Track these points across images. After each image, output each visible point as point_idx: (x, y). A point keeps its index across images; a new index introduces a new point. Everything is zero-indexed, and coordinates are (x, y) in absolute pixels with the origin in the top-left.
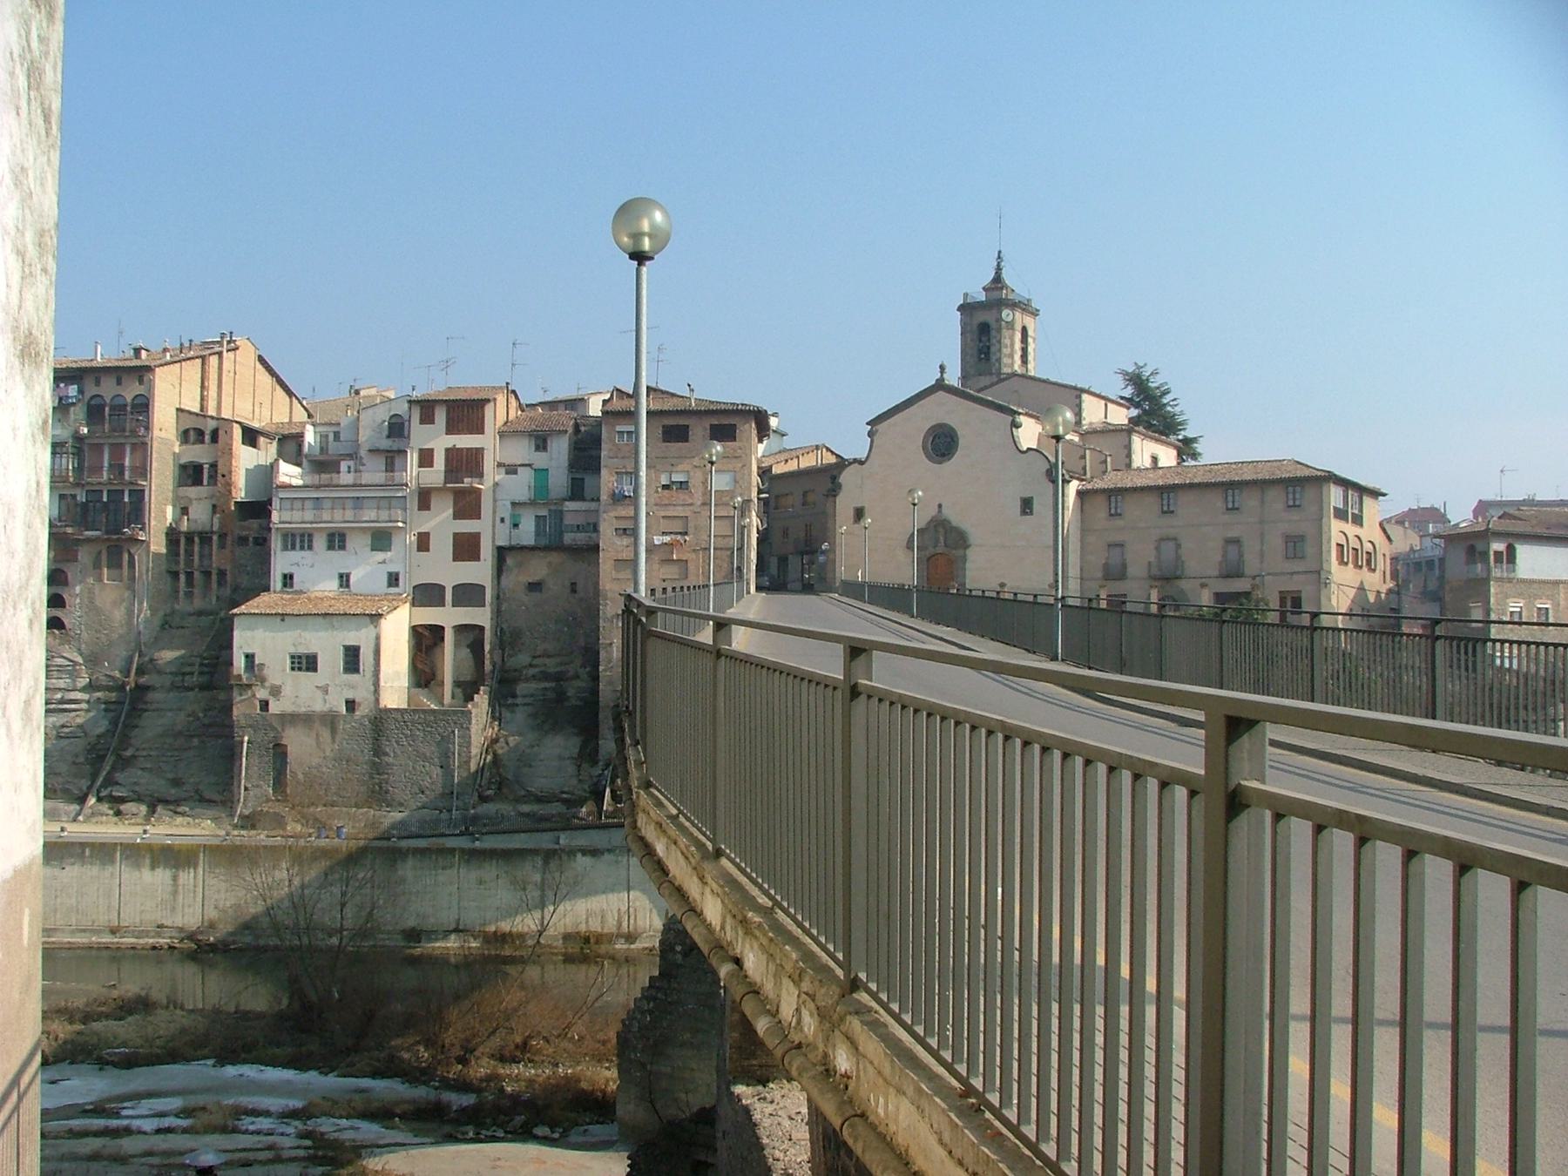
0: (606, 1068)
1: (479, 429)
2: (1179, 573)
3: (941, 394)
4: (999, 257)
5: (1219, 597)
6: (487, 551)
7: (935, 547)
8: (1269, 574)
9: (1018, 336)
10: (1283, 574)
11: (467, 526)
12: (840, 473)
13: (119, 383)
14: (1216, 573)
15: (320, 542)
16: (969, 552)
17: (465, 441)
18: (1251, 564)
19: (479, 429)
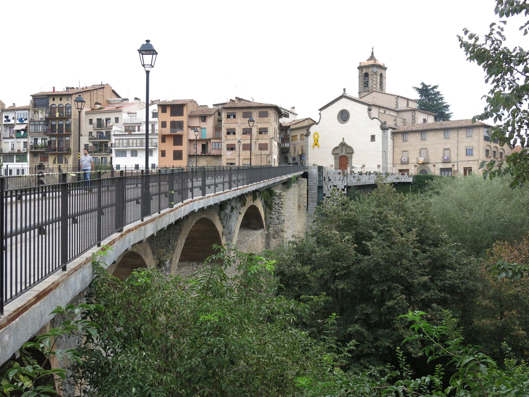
0: (211, 355)
1: (182, 114)
2: (427, 161)
3: (344, 100)
4: (373, 49)
5: (442, 170)
6: (185, 155)
7: (342, 153)
8: (460, 161)
9: (379, 77)
10: (465, 161)
11: (178, 148)
12: (310, 128)
13: (61, 100)
14: (441, 161)
15: (129, 154)
16: (353, 155)
17: (177, 119)
18: (454, 158)
19: (182, 114)
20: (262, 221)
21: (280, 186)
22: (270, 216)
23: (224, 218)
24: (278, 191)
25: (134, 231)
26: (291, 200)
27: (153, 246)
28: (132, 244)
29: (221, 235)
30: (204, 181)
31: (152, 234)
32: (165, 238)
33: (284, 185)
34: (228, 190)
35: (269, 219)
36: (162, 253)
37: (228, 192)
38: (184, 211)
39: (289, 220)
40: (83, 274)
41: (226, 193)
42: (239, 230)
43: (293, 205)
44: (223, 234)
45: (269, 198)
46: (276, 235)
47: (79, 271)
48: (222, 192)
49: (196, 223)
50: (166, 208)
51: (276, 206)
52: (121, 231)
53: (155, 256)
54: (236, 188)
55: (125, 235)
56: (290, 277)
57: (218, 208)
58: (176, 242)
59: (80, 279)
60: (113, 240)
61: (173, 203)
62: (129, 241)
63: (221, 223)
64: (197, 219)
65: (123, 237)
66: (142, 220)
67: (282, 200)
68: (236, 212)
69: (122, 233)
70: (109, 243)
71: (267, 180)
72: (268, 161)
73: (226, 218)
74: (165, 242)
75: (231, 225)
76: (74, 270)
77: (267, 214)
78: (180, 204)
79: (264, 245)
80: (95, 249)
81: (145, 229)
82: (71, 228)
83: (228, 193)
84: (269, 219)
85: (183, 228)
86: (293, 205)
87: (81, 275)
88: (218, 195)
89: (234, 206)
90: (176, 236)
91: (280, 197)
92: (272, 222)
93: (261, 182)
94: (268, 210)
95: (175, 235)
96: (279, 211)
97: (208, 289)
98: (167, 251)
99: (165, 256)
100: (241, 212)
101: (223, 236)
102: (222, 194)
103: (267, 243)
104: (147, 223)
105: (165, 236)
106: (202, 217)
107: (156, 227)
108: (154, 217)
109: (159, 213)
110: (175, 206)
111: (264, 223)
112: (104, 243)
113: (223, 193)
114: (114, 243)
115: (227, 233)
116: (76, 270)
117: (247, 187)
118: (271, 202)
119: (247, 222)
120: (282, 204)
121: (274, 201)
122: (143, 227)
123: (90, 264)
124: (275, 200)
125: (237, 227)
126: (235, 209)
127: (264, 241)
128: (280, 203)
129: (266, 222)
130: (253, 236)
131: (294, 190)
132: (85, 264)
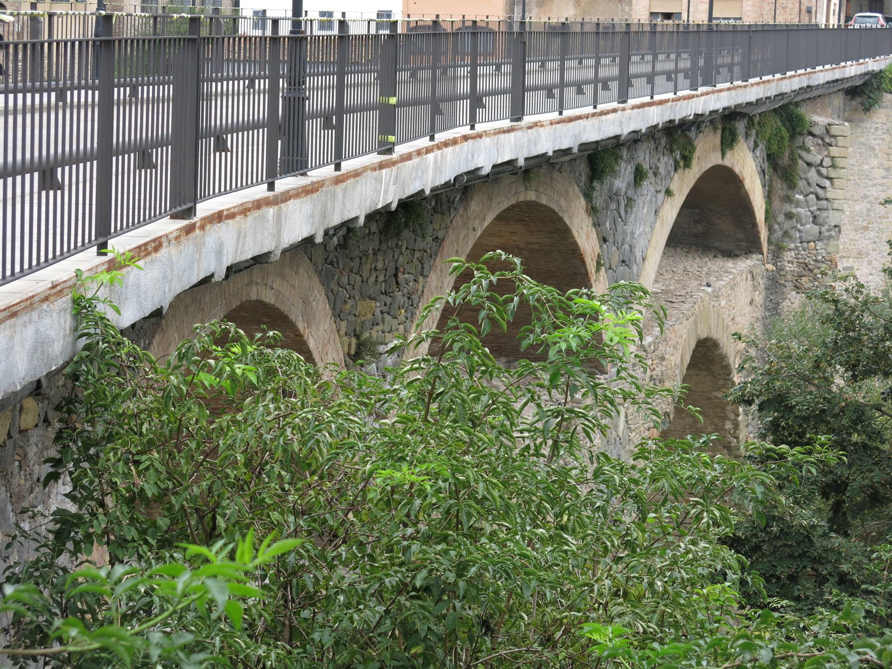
20: (754, 225)
21: (838, 101)
22: (788, 208)
23: (607, 208)
24: (819, 119)
25: (238, 218)
26: (876, 156)
27: (334, 286)
28: (229, 260)
29: (591, 266)
30: (519, 74)
31: (305, 234)
32: (380, 265)
33: (853, 98)
34: (615, 105)
35: (781, 218)
36: (370, 316)
37: (614, 111)
38: (437, 169)
39: (866, 228)
40: (37, 331)
41: (602, 113)
42: (664, 253)
43: (882, 172)
44: (599, 265)
45: (786, 143)
46: (804, 279)
47: (24, 318)
48: (590, 110)
49: (500, 218)
50: (365, 153)
51: (812, 174)
52: (189, 212)
53: (344, 324)
54: (647, 99)
55: (202, 227)
56: (806, 419)
57: (583, 168)
58: (421, 279)
59: (29, 344)
60: (154, 241)
61: (392, 139)
62: (219, 252)
63: (594, 225)
64: (505, 206)
65: (191, 236)
66: (271, 187)
67: (834, 151)
68: (652, 189)
69: (193, 221)
70: (139, 247)
71: (778, 76)
72: (804, 7)
73: (613, 206)
74: (381, 278)
75: (633, 234)
76: (6, 313)
77: (776, 203)
78: (424, 142)
79: (759, 314)
80: (88, 259)
81: (279, 216)
82: (36, 201)
83: (611, 116)
84: (781, 218)
85: (451, 235)
86: (884, 173)
87: (30, 331)
88: (571, 120)
89: (646, 166)
90: (421, 261)
91: (827, 138)
92: (792, 232)
93: (751, 81)
94: (780, 186)
95: (417, 255)
96: (820, 191)
97: (433, 396)
98: (385, 309)
99: (380, 328)
100: (673, 187)
101: (598, 270)
102: (587, 117)
103: (771, 306)
104: (286, 197)
105: (380, 258)
106: (522, 198)
107: (324, 216)
108: (315, 180)
109: (338, 167)
110: (401, 150)
111: (764, 234)
112: (119, 245)
113: (594, 115)
114: (156, 249)
115: (616, 259)
116: (14, 315)
117: (693, 97)
118: (793, 159)
119: (700, 228)
120: (833, 166)
121: (804, 154)
122: (271, 211)
123: (65, 302)
124: (808, 151)
125: (653, 243)
126: (650, 175)
127: (759, 298)
128: (827, 162)
129: (770, 229)
130: (719, 279)
131: (888, 116)
132: (46, 299)
